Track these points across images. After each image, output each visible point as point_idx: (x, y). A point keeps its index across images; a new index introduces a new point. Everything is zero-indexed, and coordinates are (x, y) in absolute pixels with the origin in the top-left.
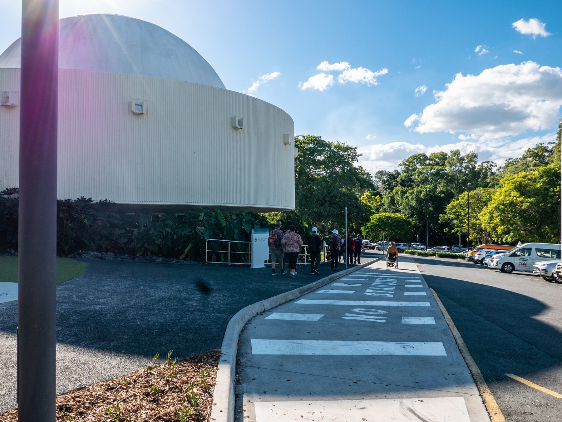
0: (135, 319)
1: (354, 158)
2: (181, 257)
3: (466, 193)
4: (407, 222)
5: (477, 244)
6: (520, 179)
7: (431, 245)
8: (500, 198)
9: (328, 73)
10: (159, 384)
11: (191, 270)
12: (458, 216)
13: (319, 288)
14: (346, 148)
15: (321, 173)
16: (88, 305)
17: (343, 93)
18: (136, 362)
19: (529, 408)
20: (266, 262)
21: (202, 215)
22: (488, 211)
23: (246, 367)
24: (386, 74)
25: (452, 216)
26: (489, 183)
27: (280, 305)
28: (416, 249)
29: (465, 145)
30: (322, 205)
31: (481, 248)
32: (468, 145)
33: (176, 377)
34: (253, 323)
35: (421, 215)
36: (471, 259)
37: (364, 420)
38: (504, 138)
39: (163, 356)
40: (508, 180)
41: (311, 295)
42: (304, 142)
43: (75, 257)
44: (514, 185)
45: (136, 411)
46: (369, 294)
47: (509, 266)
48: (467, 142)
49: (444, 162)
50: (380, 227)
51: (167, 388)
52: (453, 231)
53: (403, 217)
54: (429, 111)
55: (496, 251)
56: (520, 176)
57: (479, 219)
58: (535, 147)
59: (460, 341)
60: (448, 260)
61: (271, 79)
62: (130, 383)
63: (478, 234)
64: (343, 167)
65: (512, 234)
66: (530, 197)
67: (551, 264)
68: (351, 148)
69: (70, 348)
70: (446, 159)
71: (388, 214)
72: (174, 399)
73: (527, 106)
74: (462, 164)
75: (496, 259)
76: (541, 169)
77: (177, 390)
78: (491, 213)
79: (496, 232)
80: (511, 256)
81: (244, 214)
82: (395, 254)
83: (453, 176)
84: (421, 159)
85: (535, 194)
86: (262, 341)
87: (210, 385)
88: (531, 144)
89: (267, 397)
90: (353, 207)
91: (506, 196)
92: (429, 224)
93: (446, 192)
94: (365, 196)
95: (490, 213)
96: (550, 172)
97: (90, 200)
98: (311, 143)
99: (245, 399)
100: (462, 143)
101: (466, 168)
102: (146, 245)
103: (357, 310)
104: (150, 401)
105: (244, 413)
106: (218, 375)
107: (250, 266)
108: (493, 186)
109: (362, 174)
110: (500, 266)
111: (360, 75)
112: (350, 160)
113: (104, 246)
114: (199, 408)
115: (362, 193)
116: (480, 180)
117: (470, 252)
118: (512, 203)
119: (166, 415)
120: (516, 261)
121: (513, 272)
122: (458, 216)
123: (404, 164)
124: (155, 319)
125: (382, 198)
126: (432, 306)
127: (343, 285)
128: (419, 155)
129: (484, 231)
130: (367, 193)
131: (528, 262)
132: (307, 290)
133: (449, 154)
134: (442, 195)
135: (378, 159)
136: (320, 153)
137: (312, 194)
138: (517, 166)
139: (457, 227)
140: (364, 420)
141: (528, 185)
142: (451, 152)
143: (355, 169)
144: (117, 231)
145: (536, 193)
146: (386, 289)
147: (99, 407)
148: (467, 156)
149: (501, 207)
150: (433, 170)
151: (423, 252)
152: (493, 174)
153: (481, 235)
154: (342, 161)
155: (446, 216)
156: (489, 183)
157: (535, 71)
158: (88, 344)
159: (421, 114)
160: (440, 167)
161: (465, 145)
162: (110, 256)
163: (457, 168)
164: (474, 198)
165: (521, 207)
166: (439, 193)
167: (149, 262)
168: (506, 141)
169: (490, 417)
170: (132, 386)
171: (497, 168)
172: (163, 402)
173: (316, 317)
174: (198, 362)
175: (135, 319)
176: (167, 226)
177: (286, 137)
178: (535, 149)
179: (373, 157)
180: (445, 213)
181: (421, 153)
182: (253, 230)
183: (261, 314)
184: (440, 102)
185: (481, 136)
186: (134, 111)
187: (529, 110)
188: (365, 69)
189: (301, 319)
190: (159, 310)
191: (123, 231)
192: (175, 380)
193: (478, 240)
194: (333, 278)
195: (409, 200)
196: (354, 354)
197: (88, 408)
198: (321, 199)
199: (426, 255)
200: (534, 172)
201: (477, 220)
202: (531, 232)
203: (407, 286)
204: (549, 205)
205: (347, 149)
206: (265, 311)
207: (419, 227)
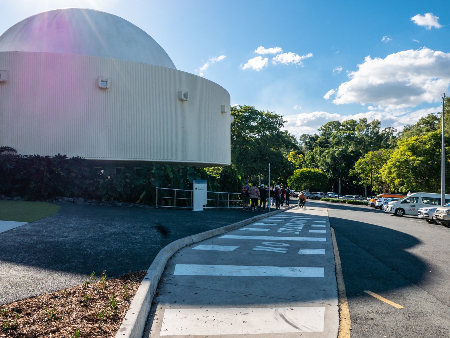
0: (87, 248)
1: (281, 124)
2: (137, 202)
3: (370, 152)
4: (323, 176)
5: (379, 193)
6: (413, 142)
7: (343, 194)
8: (397, 157)
9: (264, 56)
10: (91, 294)
11: (132, 211)
12: (363, 171)
13: (242, 227)
14: (275, 116)
15: (255, 136)
16: (53, 237)
17: (275, 71)
18: (79, 279)
19: (372, 315)
20: (204, 206)
21: (154, 168)
22: (387, 167)
23: (166, 284)
24: (311, 57)
25: (359, 171)
26: (389, 145)
27: (207, 239)
28: (330, 197)
29: (373, 114)
30: (255, 161)
31: (381, 197)
32: (375, 114)
33: (107, 290)
34: (181, 253)
35: (335, 170)
36: (373, 205)
37: (244, 322)
38: (406, 109)
39: (98, 275)
40: (403, 142)
41: (235, 232)
42: (241, 111)
43: (53, 201)
44: (408, 147)
45: (70, 313)
46: (280, 231)
47: (401, 211)
48: (375, 112)
49: (354, 128)
50: (302, 179)
51: (97, 297)
52: (360, 183)
53: (321, 171)
54: (343, 88)
55: (392, 199)
56: (412, 140)
57: (380, 174)
58: (427, 116)
59: (339, 267)
60: (354, 206)
61: (218, 60)
62: (70, 293)
63: (379, 185)
64: (272, 131)
65: (406, 185)
66: (420, 156)
67: (432, 209)
68: (278, 116)
69: (32, 269)
70: (356, 125)
71: (308, 169)
72: (101, 305)
73: (424, 83)
74: (368, 129)
75: (390, 205)
76: (430, 134)
77: (105, 299)
78: (390, 168)
79: (394, 184)
80: (402, 203)
81: (188, 168)
82: (304, 199)
83: (361, 139)
84: (336, 126)
85: (424, 154)
86: (184, 266)
87: (132, 296)
88: (424, 114)
89: (176, 305)
90: (280, 163)
91: (402, 155)
92: (342, 177)
93: (355, 152)
94: (291, 155)
95: (388, 168)
96: (437, 137)
97: (65, 156)
98: (246, 112)
99: (159, 306)
100: (370, 113)
101: (372, 132)
102: (110, 192)
103: (266, 243)
104: (82, 306)
105: (155, 316)
106: (139, 289)
107: (192, 209)
108: (393, 147)
109: (287, 137)
110: (393, 211)
111: (289, 58)
112: (278, 125)
113: (77, 193)
114: (117, 311)
115: (289, 152)
116: (382, 142)
117: (372, 200)
118: (406, 161)
119: (91, 316)
120: (406, 207)
121: (404, 216)
122: (363, 171)
123: (322, 129)
124: (103, 248)
125: (304, 156)
126: (327, 241)
127: (263, 224)
128: (334, 122)
129: (384, 183)
130: (292, 152)
131: (416, 208)
132: (232, 228)
133: (358, 121)
134: (352, 154)
135: (303, 125)
136: (254, 120)
137: (247, 152)
138: (412, 131)
139: (363, 180)
140: (244, 322)
141: (419, 147)
142: (360, 119)
143: (282, 133)
144: (87, 182)
145: (425, 152)
146: (296, 228)
147: (43, 310)
148: (373, 123)
149: (398, 164)
150: (345, 134)
151: (336, 199)
152: (394, 137)
153: (382, 186)
154: (271, 127)
155: (354, 171)
156: (390, 145)
157: (430, 56)
158: (46, 266)
159: (336, 89)
160: (351, 132)
161: (373, 114)
162: (81, 200)
163: (364, 132)
164: (377, 157)
165: (413, 164)
166: (350, 153)
167: (111, 205)
168: (408, 111)
169: (340, 321)
170: (71, 296)
171: (398, 132)
172: (92, 307)
173: (232, 248)
174: (127, 279)
175: (87, 248)
176: (126, 177)
177: (223, 107)
178: (427, 118)
179: (299, 123)
180: (354, 169)
181: (336, 120)
182: (194, 181)
183: (190, 245)
184: (352, 80)
185: (386, 107)
186: (100, 86)
187: (425, 87)
188: (293, 54)
189: (220, 250)
190: (108, 241)
191: (92, 181)
192: (106, 292)
193: (380, 190)
194: (255, 219)
195: (326, 158)
196: (253, 275)
197: (35, 311)
198: (254, 157)
199: (338, 202)
200: (424, 136)
201: (379, 174)
202: (421, 184)
203: (313, 225)
204: (436, 163)
205: (276, 117)
206: (193, 243)
207: (333, 179)
